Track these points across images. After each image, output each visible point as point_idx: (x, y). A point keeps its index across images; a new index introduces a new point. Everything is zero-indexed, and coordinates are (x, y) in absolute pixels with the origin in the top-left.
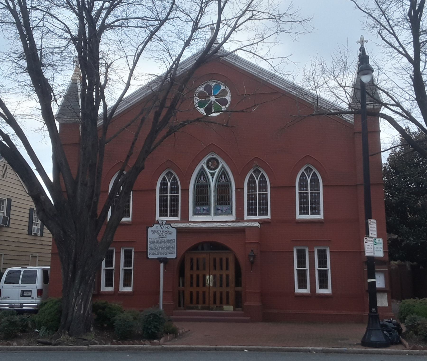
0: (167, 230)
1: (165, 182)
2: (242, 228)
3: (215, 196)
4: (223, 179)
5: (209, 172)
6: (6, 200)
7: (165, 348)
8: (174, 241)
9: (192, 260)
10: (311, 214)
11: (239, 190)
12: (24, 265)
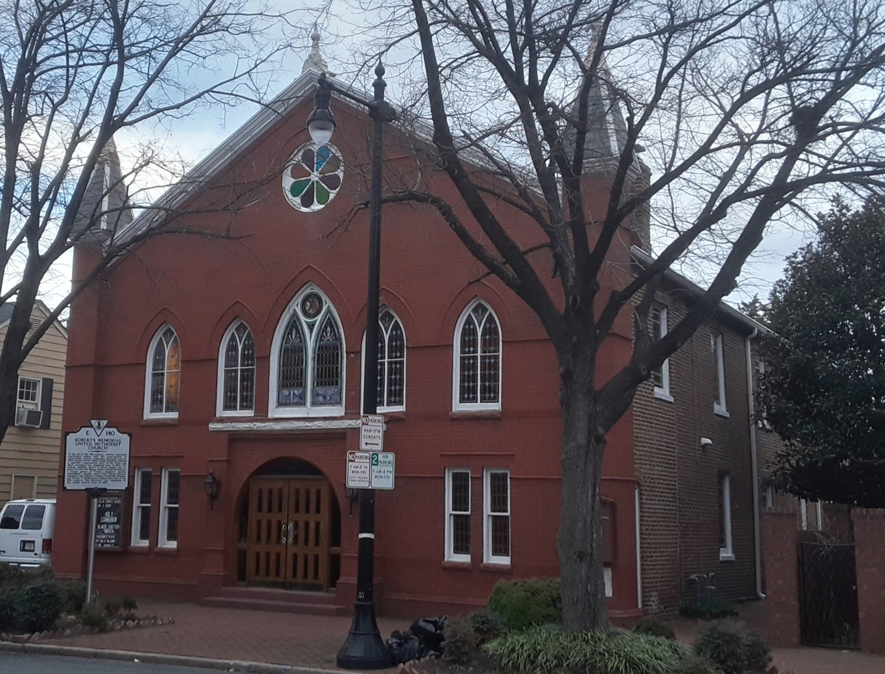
0: (109, 437)
1: (472, 327)
2: (341, 431)
3: (313, 369)
4: (329, 335)
5: (306, 322)
6: (39, 381)
7: (29, 648)
8: (123, 457)
9: (260, 491)
10: (481, 402)
11: (352, 356)
12: (30, 498)
